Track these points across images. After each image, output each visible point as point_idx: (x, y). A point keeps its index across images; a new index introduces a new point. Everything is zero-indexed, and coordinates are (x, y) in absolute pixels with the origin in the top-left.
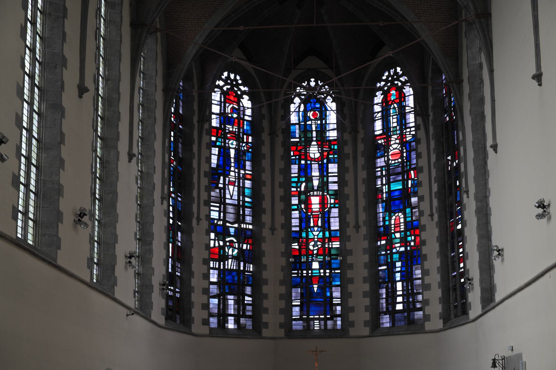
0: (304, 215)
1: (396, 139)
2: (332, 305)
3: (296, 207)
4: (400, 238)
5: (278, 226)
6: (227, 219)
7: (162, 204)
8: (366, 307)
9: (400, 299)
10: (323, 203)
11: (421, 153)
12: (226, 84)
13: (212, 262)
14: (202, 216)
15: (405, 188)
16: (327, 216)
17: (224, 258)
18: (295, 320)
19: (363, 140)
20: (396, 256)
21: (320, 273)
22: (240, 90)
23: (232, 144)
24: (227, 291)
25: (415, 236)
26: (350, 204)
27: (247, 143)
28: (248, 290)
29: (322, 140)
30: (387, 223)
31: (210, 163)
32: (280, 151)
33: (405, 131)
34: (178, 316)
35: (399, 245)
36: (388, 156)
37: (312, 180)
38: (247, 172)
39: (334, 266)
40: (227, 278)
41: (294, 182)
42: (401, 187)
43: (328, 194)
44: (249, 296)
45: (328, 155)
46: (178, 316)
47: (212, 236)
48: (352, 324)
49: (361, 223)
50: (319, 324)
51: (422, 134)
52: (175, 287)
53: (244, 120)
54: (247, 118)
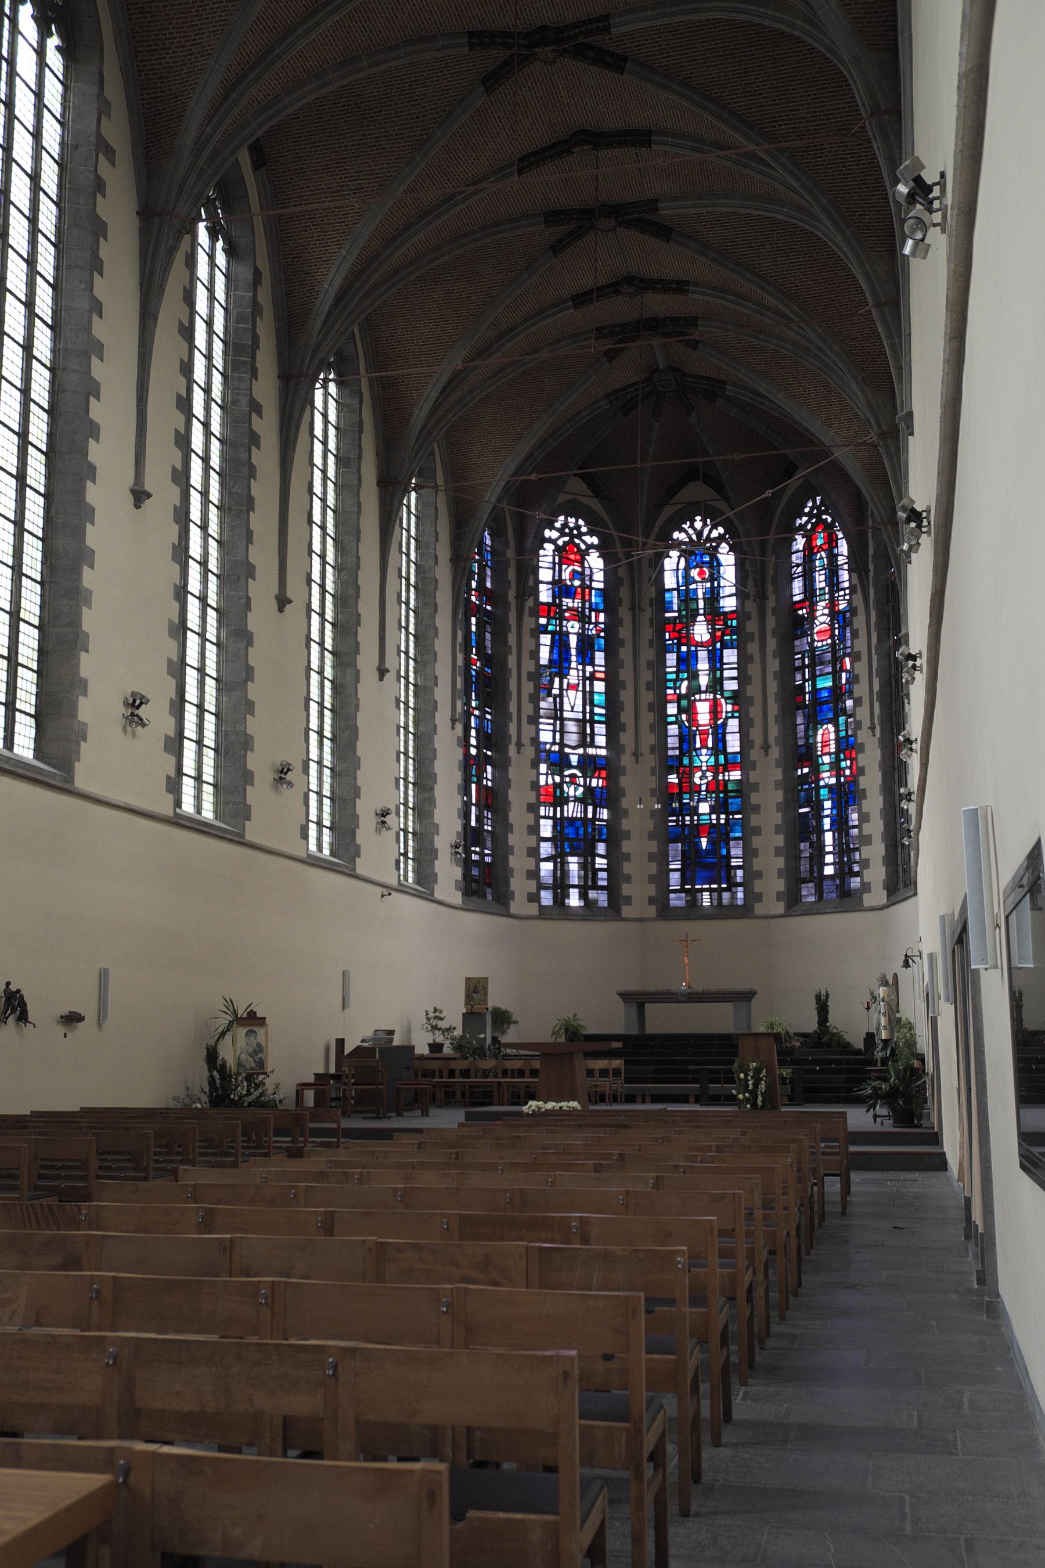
1: (825, 608)
2: (730, 868)
3: (673, 719)
4: (830, 763)
5: (645, 748)
6: (565, 742)
8: (779, 870)
9: (829, 859)
10: (715, 710)
11: (858, 629)
14: (526, 740)
15: (836, 687)
17: (561, 801)
18: (674, 891)
19: (774, 611)
21: (711, 819)
22: (584, 542)
23: (572, 627)
24: (568, 850)
26: (755, 712)
27: (597, 623)
28: (601, 848)
29: (714, 613)
31: (538, 658)
32: (647, 633)
33: (836, 595)
34: (489, 891)
35: (828, 774)
36: (812, 635)
37: (698, 675)
38: (597, 668)
39: (732, 808)
40: (566, 831)
41: (671, 680)
42: (830, 684)
43: (723, 697)
45: (723, 635)
46: (489, 891)
47: (543, 768)
48: (758, 897)
49: (772, 741)
50: (711, 898)
52: (483, 848)
53: (591, 588)
54: (595, 585)
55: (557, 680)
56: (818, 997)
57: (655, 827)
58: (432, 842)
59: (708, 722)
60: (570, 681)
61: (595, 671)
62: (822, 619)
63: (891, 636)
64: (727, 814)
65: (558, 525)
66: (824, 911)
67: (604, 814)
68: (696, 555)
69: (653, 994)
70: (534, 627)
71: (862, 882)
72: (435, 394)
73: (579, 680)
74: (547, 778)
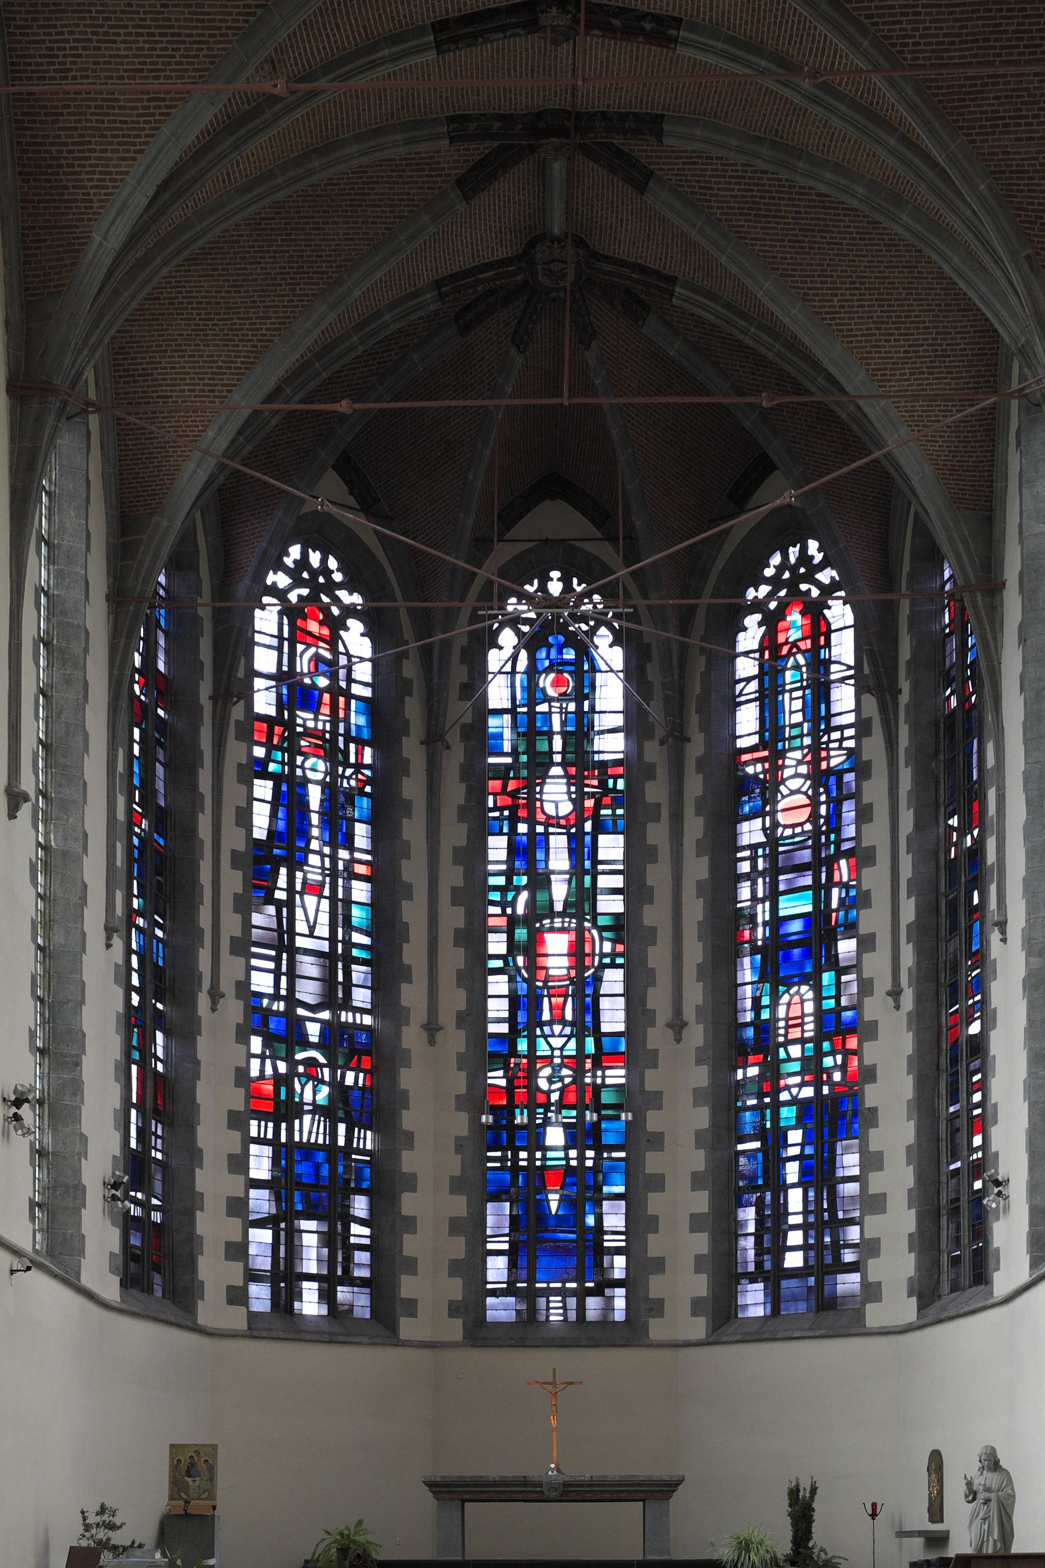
0: (522, 988)
1: (800, 763)
2: (600, 1251)
3: (499, 964)
5: (447, 1018)
6: (298, 996)
7: (108, 946)
8: (698, 1258)
9: (795, 1238)
10: (577, 952)
11: (871, 805)
12: (298, 582)
13: (254, 1123)
14: (227, 986)
16: (589, 991)
18: (494, 1293)
19: (701, 765)
20: (788, 1114)
21: (567, 1158)
23: (314, 770)
24: (299, 1207)
25: (848, 1054)
26: (659, 957)
27: (359, 766)
28: (360, 1205)
30: (765, 1015)
31: (249, 827)
32: (454, 792)
33: (825, 739)
34: (157, 1278)
35: (797, 1079)
37: (549, 882)
39: (608, 1139)
41: (496, 888)
42: (809, 908)
44: (362, 1222)
46: (157, 1278)
48: (657, 1308)
49: (689, 1013)
51: (875, 749)
53: (349, 696)
54: (357, 690)
55: (283, 871)
56: (794, 1493)
57: (462, 1168)
58: (77, 1172)
59: (564, 972)
60: (309, 876)
61: (353, 861)
62: (794, 784)
63: (942, 819)
64: (599, 1148)
65: (289, 561)
66: (787, 1334)
67: (368, 1140)
68: (549, 646)
69: (495, 1484)
70: (244, 761)
71: (864, 1283)
72: (141, 200)
73: (324, 876)
74: (263, 1064)
